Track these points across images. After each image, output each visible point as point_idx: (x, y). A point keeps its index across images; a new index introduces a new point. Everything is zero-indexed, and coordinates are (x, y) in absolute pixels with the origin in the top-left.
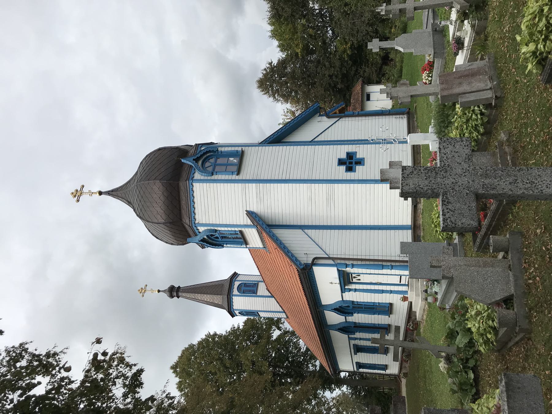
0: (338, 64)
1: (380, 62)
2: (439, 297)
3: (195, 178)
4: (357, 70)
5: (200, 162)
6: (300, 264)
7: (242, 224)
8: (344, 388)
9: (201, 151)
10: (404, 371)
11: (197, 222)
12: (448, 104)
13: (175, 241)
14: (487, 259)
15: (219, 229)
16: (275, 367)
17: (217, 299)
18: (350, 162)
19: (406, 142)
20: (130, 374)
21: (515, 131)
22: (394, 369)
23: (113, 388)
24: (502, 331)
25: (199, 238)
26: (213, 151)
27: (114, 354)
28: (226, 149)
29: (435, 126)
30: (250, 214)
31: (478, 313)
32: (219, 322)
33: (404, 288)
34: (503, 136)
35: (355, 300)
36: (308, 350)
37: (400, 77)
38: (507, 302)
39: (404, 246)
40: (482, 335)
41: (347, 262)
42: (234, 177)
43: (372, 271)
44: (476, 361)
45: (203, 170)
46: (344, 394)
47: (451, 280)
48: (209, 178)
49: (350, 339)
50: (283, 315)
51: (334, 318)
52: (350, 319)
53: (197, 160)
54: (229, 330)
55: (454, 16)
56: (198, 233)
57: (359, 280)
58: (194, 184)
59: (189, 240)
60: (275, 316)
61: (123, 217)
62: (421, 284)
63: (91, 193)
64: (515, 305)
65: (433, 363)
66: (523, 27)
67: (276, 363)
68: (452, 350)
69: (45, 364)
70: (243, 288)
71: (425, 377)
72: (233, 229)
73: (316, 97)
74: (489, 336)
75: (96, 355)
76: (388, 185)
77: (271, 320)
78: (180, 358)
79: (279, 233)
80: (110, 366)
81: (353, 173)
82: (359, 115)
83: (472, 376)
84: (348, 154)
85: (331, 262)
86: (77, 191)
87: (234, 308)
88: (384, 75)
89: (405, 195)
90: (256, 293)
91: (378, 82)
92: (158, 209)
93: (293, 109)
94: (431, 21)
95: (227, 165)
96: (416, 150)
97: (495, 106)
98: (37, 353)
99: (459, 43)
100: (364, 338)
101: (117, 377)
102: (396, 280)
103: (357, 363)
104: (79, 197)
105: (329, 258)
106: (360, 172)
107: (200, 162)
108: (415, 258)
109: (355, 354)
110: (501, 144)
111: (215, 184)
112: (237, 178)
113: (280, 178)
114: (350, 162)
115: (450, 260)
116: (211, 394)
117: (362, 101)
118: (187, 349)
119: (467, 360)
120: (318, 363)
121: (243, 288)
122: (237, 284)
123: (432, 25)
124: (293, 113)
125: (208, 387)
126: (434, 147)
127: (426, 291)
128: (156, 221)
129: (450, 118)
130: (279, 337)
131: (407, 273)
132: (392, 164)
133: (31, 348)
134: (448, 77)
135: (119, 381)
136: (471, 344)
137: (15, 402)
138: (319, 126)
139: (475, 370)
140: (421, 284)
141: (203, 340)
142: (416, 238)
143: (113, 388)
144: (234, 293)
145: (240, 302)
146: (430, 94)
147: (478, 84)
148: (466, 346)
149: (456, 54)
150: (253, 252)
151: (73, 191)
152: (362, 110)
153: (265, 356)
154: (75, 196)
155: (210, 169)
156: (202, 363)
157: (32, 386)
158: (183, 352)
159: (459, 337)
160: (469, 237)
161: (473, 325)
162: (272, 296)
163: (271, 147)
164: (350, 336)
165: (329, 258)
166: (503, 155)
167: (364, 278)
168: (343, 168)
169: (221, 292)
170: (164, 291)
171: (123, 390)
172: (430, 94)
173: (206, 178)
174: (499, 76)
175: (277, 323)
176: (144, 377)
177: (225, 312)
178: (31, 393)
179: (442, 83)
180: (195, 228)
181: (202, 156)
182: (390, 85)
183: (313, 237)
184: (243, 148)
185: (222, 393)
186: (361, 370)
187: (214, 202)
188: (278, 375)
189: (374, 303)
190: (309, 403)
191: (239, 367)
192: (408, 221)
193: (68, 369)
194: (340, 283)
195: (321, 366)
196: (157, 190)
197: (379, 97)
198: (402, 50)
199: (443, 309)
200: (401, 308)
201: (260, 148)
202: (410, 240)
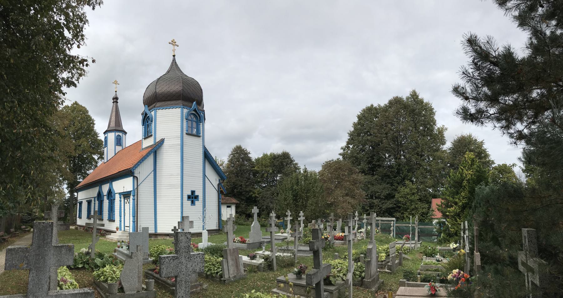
0: (248, 189)
1: (248, 213)
2: (120, 249)
4: (243, 200)
5: (194, 112)
8: (68, 195)
10: (79, 227)
12: (223, 253)
14: (142, 278)
16: (78, 157)
17: (113, 124)
18: (193, 197)
19: (203, 230)
20: (74, 80)
21: (208, 293)
22: (80, 222)
23: (67, 72)
24: (105, 285)
25: (148, 112)
27: (84, 71)
28: (201, 127)
29: (212, 246)
30: (162, 141)
31: (114, 272)
32: (100, 126)
33: (123, 229)
34: (205, 286)
36: (88, 175)
37: (239, 225)
38: (121, 289)
39: (147, 229)
40: (103, 273)
41: (136, 196)
42: (185, 132)
43: (131, 211)
44: (88, 269)
45: (189, 114)
46: (65, 195)
47: (130, 257)
50: (106, 161)
52: (105, 198)
53: (195, 110)
54: (97, 131)
55: (267, 253)
59: (147, 106)
60: (105, 156)
61: (160, 69)
62: (126, 238)
64: (120, 294)
65: (84, 244)
66: (258, 293)
67: (80, 157)
68: (93, 256)
69: (78, 35)
71: (76, 239)
73: (230, 177)
74: (102, 277)
75: (86, 61)
76: (180, 220)
77: (103, 154)
78: (81, 106)
79: (151, 158)
80: (77, 69)
82: (219, 202)
83: (80, 266)
84: (198, 196)
85: (136, 187)
88: (240, 215)
89: (175, 229)
91: (236, 212)
92: (163, 89)
93: (224, 165)
94: (266, 240)
95: (192, 127)
96: (199, 235)
97: (221, 280)
98: (84, 30)
99: (253, 257)
100: (95, 206)
101: (72, 73)
102: (127, 224)
103: (82, 202)
104: (172, 44)
105: (138, 186)
106: (187, 203)
107: (194, 112)
108: (139, 235)
110: (201, 285)
112: (184, 133)
115: (140, 257)
116: (64, 124)
117: (227, 203)
118: (86, 109)
119: (88, 264)
120: (81, 180)
122: (121, 134)
123: (264, 242)
124: (222, 165)
125: (67, 122)
126: (201, 245)
127: (123, 242)
128: (157, 87)
129: (216, 255)
130: (94, 159)
131: (131, 231)
132: (192, 222)
133: (86, 26)
134: (237, 251)
135: (70, 75)
136: (97, 267)
137: (60, 21)
138: (213, 179)
139: (83, 268)
140: (126, 238)
141: (91, 118)
142: (151, 235)
143: (67, 72)
145: (112, 137)
146: (228, 243)
147: (232, 270)
148: (95, 263)
149: (248, 256)
151: (175, 41)
152: (222, 203)
153: (84, 152)
155: (190, 118)
156: (80, 118)
157: (69, 29)
158: (84, 107)
159: (100, 260)
160: (153, 267)
161: (107, 268)
162: (115, 154)
165: (138, 186)
166: (196, 287)
167: (127, 206)
168: (190, 193)
169: (116, 127)
170: (116, 94)
171: (65, 77)
172: (228, 243)
174: (235, 281)
175: (101, 157)
176: (72, 88)
177: (106, 129)
178: (65, 29)
179: (233, 249)
181: (197, 113)
182: (234, 220)
185: (64, 129)
186: (78, 204)
187: (169, 120)
188: (74, 159)
190: (61, 176)
191: (78, 138)
192: (159, 231)
193: (78, 47)
195: (80, 182)
196: (176, 88)
197: (229, 213)
198: (252, 225)
199: (115, 251)
200: (112, 226)
202: (150, 232)
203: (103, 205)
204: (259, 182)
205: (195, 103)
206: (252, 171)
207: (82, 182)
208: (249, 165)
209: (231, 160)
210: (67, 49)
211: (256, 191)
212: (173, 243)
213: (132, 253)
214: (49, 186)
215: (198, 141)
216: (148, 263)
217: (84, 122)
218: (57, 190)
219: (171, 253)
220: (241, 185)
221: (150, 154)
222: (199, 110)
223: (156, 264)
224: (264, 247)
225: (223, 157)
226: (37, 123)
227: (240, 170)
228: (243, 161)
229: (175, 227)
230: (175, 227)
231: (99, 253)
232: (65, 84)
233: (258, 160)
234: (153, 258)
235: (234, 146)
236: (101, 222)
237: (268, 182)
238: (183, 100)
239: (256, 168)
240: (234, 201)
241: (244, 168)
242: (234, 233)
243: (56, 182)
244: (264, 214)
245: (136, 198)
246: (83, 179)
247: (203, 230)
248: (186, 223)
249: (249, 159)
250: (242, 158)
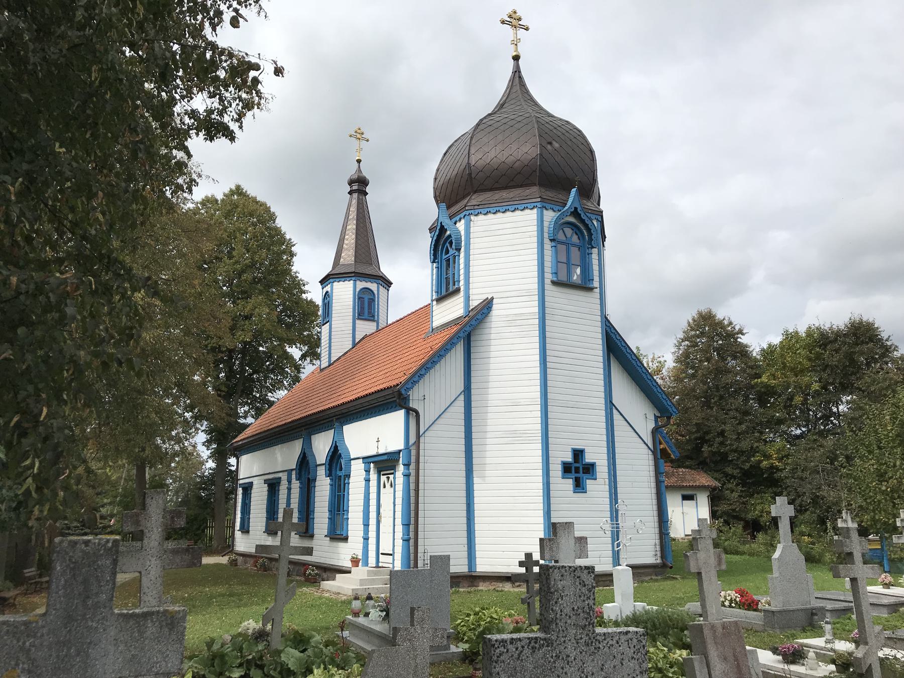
0: (745, 445)
1: (750, 516)
2: (361, 620)
4: (734, 477)
5: (572, 219)
6: (408, 389)
8: (211, 464)
10: (240, 559)
11: (472, 217)
13: (441, 183)
15: (462, 255)
16: (243, 351)
18: (578, 469)
20: (226, 119)
22: (243, 544)
23: (205, 94)
25: (447, 222)
26: (591, 239)
28: (595, 262)
29: (647, 612)
30: (487, 306)
33: (372, 561)
36: (271, 404)
42: (549, 277)
43: (399, 508)
45: (560, 225)
46: (202, 463)
47: (389, 640)
48: (546, 235)
49: (289, 472)
50: (325, 363)
52: (321, 472)
53: (575, 213)
54: (300, 276)
55: (843, 646)
56: (454, 220)
57: (385, 487)
58: (535, 210)
60: (323, 350)
62: (380, 588)
65: (255, 608)
68: (276, 642)
70: (366, 297)
73: (686, 410)
78: (255, 200)
79: (458, 353)
81: (560, 473)
82: (658, 483)
84: (593, 465)
85: (412, 440)
86: (520, 19)
87: (335, 284)
88: (727, 523)
89: (528, 562)
90: (359, 319)
91: (714, 515)
96: (606, 579)
100: (290, 495)
101: (221, 100)
102: (385, 547)
103: (251, 484)
104: (510, 23)
105: (418, 436)
106: (563, 486)
107: (572, 219)
108: (426, 582)
109: (266, 481)
112: (548, 281)
114: (578, 469)
115: (423, 640)
116: (198, 250)
118: (267, 210)
120: (250, 420)
122: (373, 286)
123: (823, 609)
124: (659, 371)
127: (369, 598)
129: (662, 639)
130: (289, 357)
131: (398, 566)
134: (734, 635)
135: (215, 103)
138: (638, 415)
141: (282, 236)
142: (457, 580)
143: (205, 94)
144: (358, 282)
145: (344, 293)
146: (703, 606)
149: (775, 651)
153: (258, 336)
154: (510, 17)
155: (561, 236)
156: (250, 238)
158: (263, 205)
159: (296, 653)
162: (355, 345)
163: (600, 336)
164: (294, 472)
165: (418, 436)
167: (387, 493)
168: (569, 458)
172: (703, 606)
173: (546, 230)
175: (312, 353)
176: (222, 142)
180: (462, 215)
181: (583, 221)
183: (451, 409)
184: (597, 290)
185: (200, 268)
188: (231, 358)
189: (348, 511)
190: (190, 408)
191: (242, 294)
192: (483, 566)
193: (235, 23)
195: (246, 426)
196: (523, 150)
198: (776, 555)
200: (343, 554)
203: (313, 492)
204: (780, 422)
205: (574, 190)
206: (753, 387)
207: (252, 424)
208: (743, 371)
209: (686, 355)
210: (207, 24)
211: (772, 451)
212: (523, 601)
213: (395, 630)
214: (150, 437)
215: (586, 302)
216: (449, 660)
217: (260, 247)
218: (177, 448)
219: (517, 630)
220: (722, 433)
222: (587, 210)
223: (472, 662)
224: (828, 627)
225: (660, 351)
226: (95, 259)
227: (717, 388)
228: (723, 358)
229: (529, 556)
230: (529, 556)
231: (297, 632)
232: (198, 130)
233: (768, 353)
234: (463, 647)
235: (686, 316)
236: (306, 543)
237: (808, 421)
238: (541, 185)
239: (764, 379)
240: (704, 479)
241: (728, 379)
242: (721, 574)
243: (173, 427)
244: (816, 517)
246: (256, 417)
247: (616, 561)
248: (566, 546)
249: (742, 352)
250: (715, 349)
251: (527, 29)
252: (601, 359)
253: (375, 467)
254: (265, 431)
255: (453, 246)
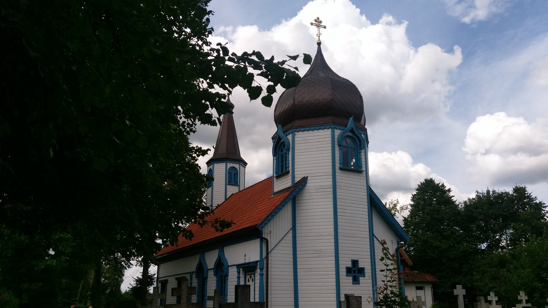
3: (336, 131)
5: (350, 134)
6: (263, 227)
7: (296, 173)
9: (360, 134)
11: (296, 133)
13: (278, 113)
15: (290, 153)
25: (282, 134)
26: (360, 145)
30: (304, 180)
35: (229, 277)
41: (265, 270)
42: (338, 165)
45: (343, 137)
48: (336, 143)
49: (191, 273)
51: (211, 259)
52: (211, 274)
53: (352, 131)
56: (286, 134)
57: (249, 281)
58: (330, 130)
59: (280, 126)
63: (319, 35)
72: (290, 165)
84: (363, 269)
85: (264, 255)
86: (321, 22)
87: (215, 164)
90: (229, 185)
103: (167, 281)
105: (268, 253)
106: (346, 281)
107: (350, 134)
109: (176, 279)
111: (330, 148)
113: (338, 207)
121: (233, 172)
122: (237, 166)
144: (228, 164)
145: (220, 170)
150: (267, 183)
154: (316, 21)
155: (344, 143)
162: (226, 199)
163: (366, 197)
165: (268, 253)
168: (350, 265)
173: (336, 140)
180: (290, 132)
181: (356, 135)
183: (286, 238)
184: (364, 173)
187: (314, 149)
189: (227, 295)
194: (245, 264)
201: (365, 188)
221: (287, 202)
225: (401, 202)
240: (429, 278)
245: (265, 273)
251: (325, 27)
252: (367, 210)
253: (243, 270)
254: (174, 251)
255: (286, 147)
